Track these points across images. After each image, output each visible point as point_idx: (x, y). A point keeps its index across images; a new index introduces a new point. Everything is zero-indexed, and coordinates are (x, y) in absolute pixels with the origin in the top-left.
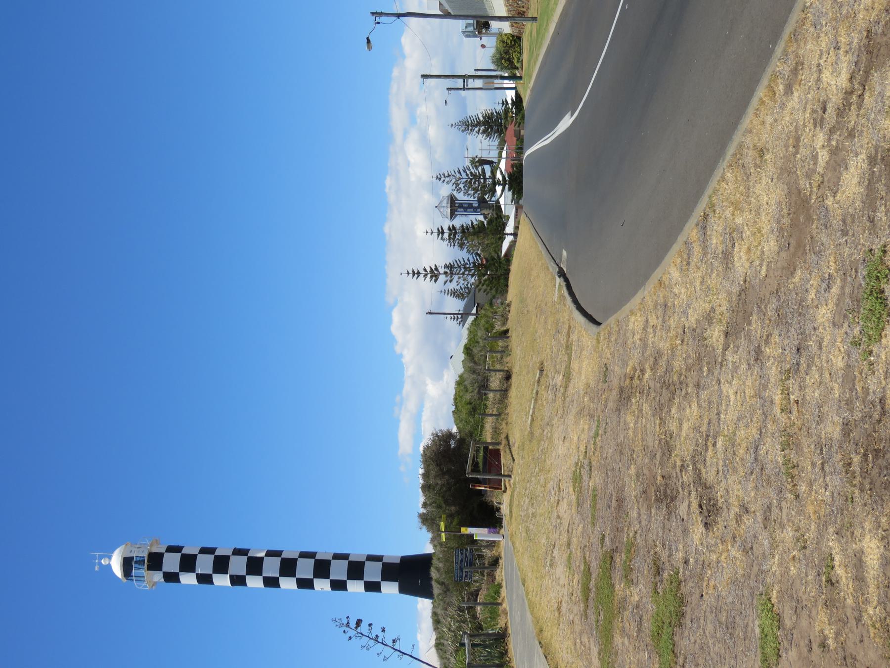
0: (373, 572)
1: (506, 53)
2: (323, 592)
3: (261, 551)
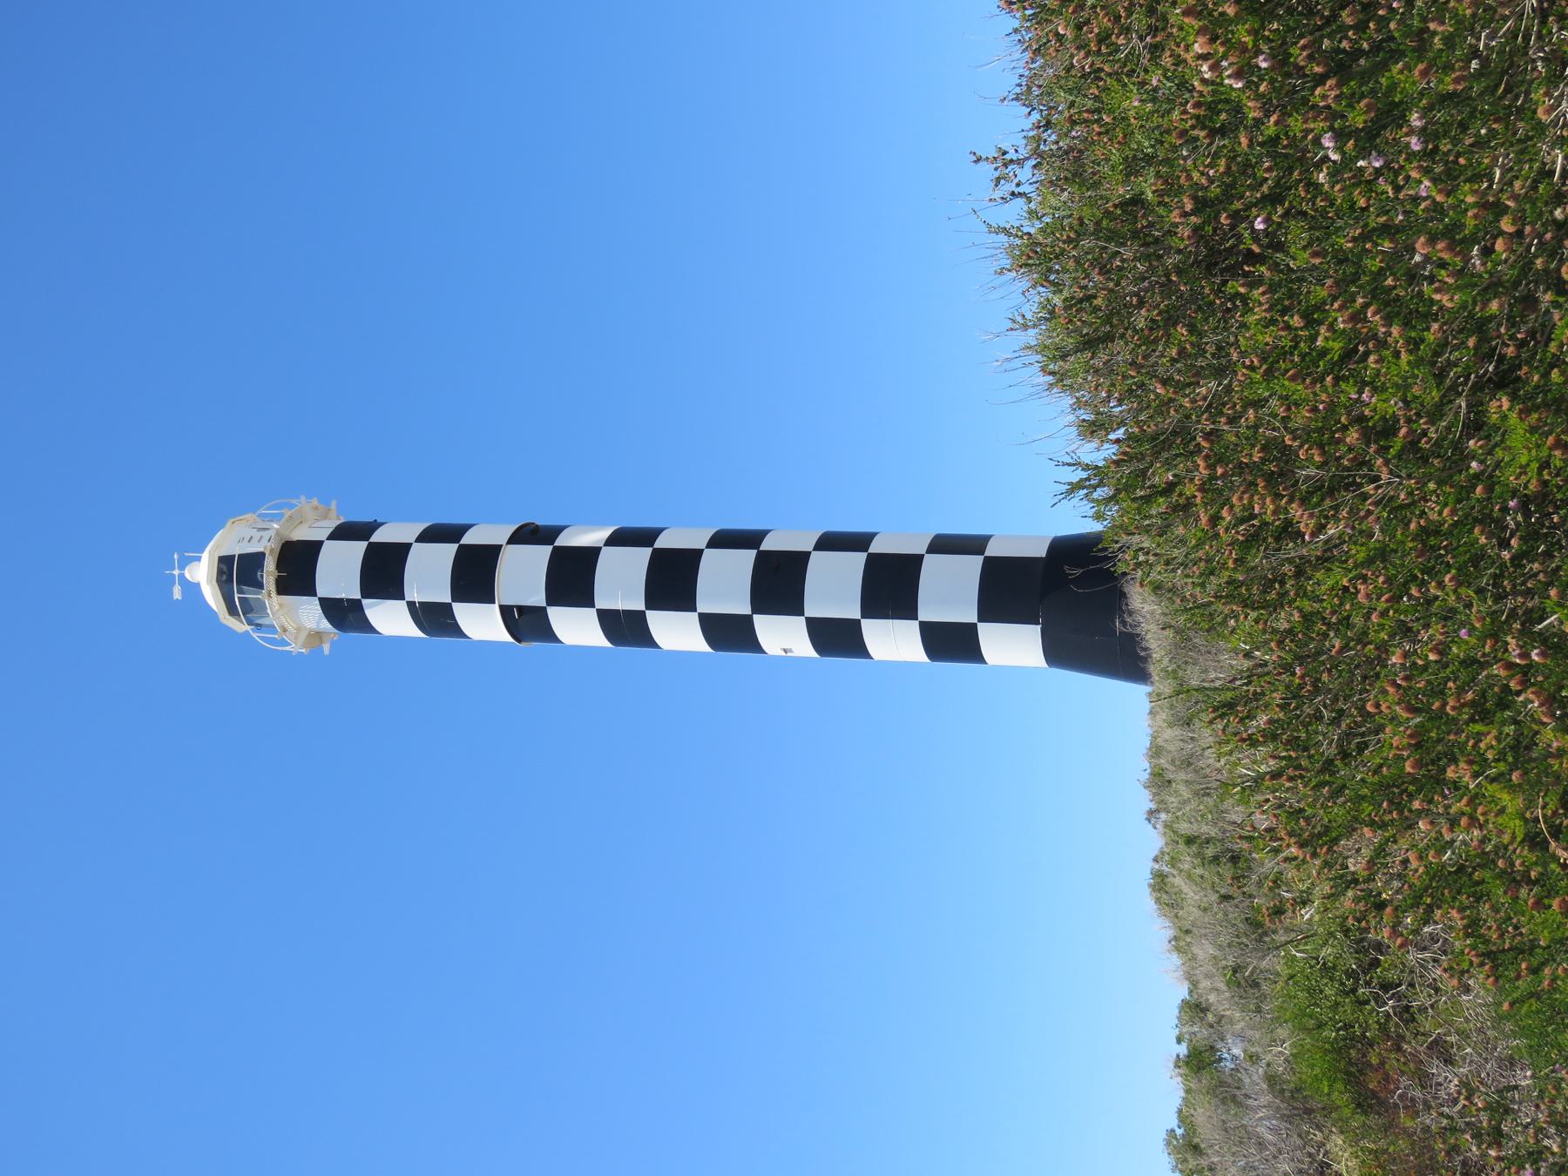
2: (788, 661)
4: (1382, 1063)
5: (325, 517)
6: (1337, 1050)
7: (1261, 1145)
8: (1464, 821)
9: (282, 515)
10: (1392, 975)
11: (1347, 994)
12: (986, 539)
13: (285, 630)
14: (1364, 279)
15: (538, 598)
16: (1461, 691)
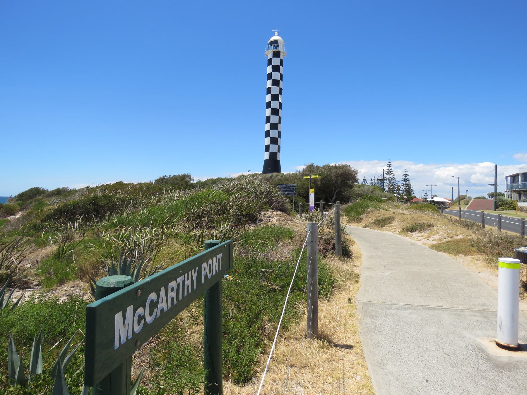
0: (273, 148)
1: (506, 203)
2: (265, 127)
12: (282, 80)
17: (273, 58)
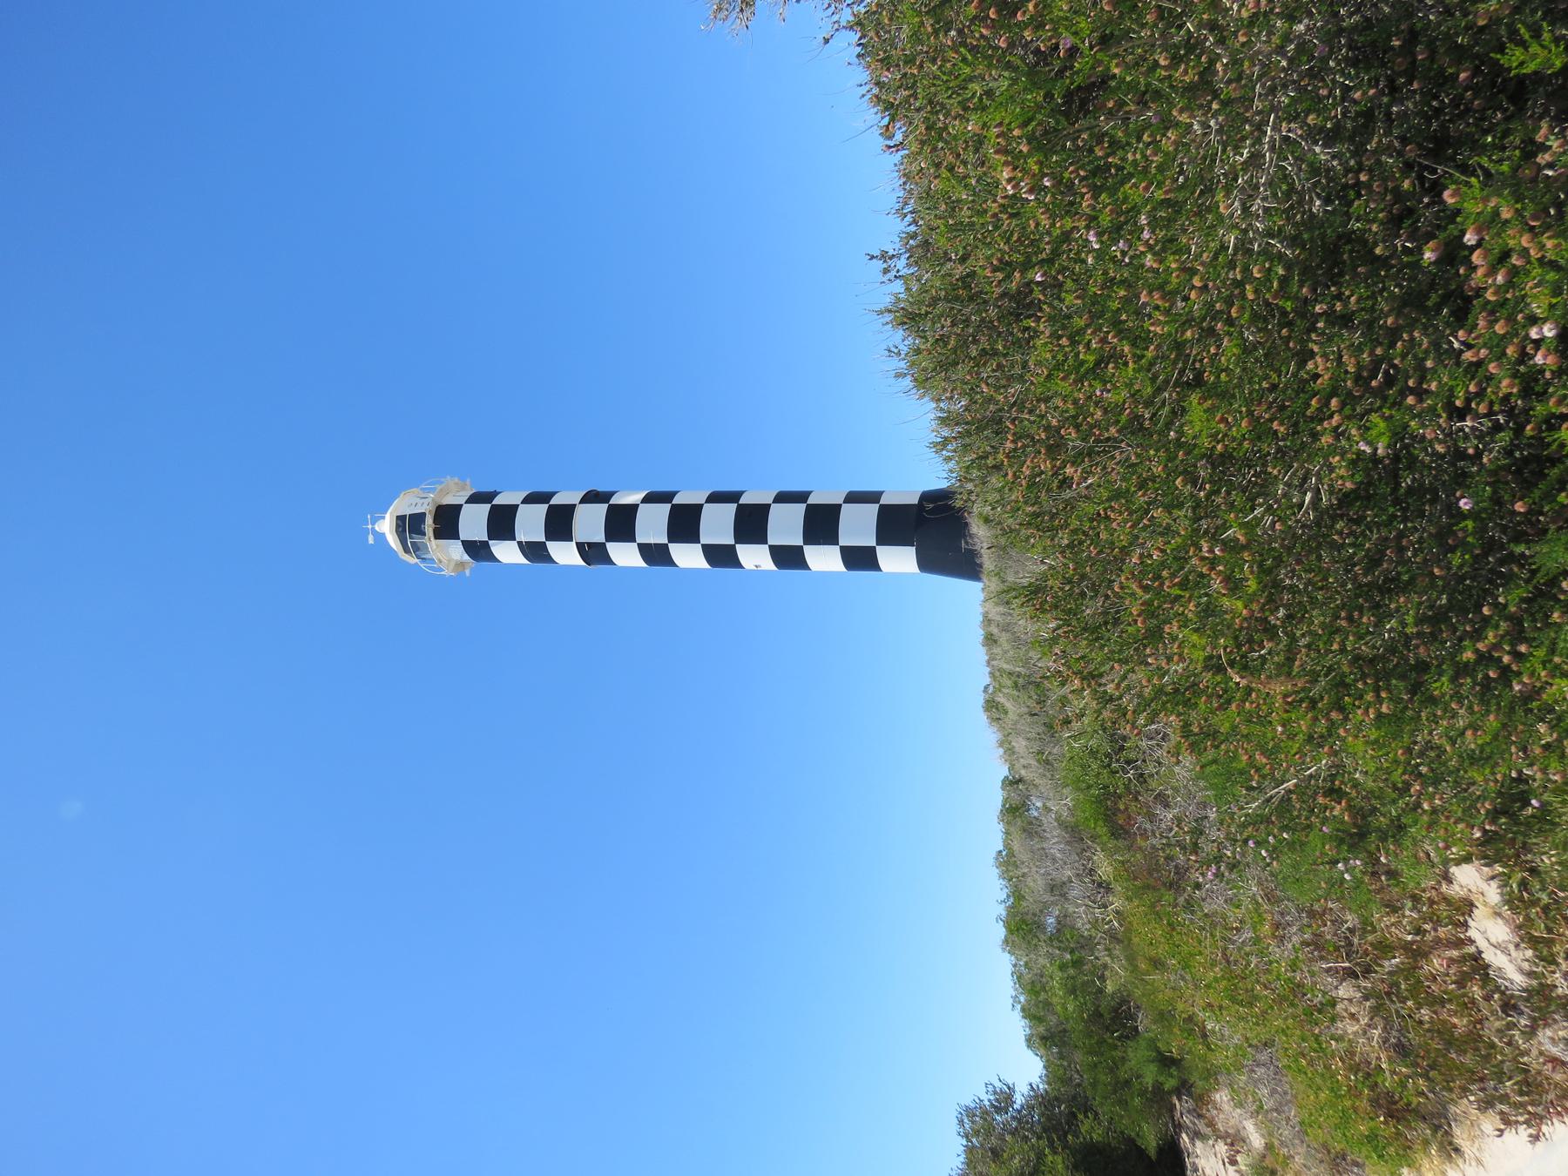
0: (858, 526)
2: (758, 573)
3: (634, 489)
4: (1126, 809)
5: (463, 489)
6: (1099, 801)
7: (1054, 860)
8: (1176, 658)
9: (435, 489)
10: (1132, 755)
11: (1105, 767)
12: (881, 493)
13: (440, 561)
14: (1108, 315)
15: (600, 537)
16: (1173, 575)
17: (463, 537)
